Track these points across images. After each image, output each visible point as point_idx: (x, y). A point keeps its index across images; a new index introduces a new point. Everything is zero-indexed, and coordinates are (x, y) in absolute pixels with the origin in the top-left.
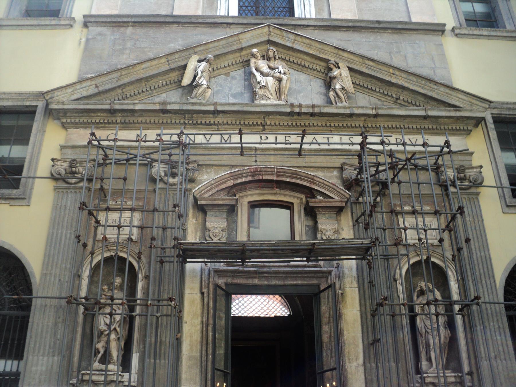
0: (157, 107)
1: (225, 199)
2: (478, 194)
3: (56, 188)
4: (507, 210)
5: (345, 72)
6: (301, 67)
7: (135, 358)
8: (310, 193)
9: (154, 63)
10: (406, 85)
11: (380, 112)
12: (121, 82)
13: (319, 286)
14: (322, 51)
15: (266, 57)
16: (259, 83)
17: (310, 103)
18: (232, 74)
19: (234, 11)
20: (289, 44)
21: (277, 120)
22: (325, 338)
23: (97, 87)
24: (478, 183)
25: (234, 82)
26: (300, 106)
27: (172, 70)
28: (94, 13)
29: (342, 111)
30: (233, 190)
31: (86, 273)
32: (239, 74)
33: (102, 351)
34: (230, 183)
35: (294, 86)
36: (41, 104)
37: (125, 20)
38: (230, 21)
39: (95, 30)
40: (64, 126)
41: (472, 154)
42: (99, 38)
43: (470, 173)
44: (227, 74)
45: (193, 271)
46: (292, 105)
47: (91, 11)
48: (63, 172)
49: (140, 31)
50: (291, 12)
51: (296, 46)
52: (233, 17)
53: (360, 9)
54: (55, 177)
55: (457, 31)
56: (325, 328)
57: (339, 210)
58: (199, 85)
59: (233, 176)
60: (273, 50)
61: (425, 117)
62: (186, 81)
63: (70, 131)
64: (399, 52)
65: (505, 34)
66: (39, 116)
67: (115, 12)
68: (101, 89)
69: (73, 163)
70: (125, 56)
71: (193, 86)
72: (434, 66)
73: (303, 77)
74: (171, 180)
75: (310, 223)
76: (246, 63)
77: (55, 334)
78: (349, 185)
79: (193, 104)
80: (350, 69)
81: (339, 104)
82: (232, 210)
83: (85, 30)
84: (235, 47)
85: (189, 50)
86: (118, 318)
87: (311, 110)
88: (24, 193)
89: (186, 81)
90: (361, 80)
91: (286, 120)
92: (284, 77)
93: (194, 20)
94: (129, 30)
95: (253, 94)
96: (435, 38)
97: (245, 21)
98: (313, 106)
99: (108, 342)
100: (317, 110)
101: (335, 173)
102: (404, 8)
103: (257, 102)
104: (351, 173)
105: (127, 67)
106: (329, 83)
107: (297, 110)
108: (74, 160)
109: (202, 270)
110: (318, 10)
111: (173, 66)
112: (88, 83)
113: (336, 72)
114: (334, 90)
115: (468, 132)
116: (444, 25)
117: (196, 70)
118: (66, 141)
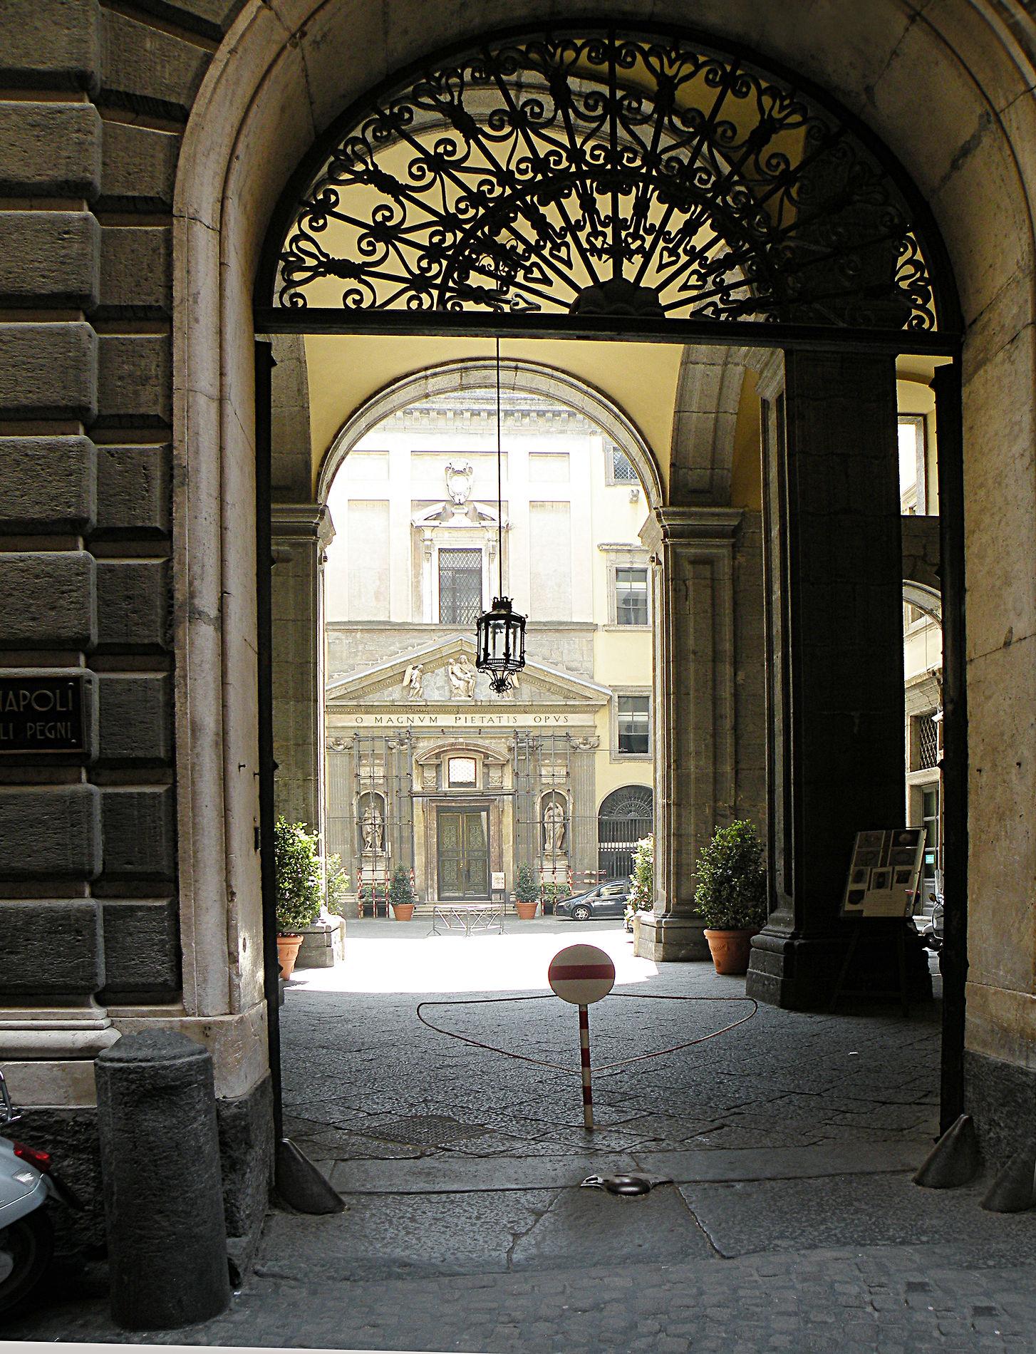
1: (435, 761)
8: (487, 756)
15: (458, 661)
30: (438, 756)
31: (354, 802)
44: (433, 672)
55: (607, 628)
94: (359, 635)
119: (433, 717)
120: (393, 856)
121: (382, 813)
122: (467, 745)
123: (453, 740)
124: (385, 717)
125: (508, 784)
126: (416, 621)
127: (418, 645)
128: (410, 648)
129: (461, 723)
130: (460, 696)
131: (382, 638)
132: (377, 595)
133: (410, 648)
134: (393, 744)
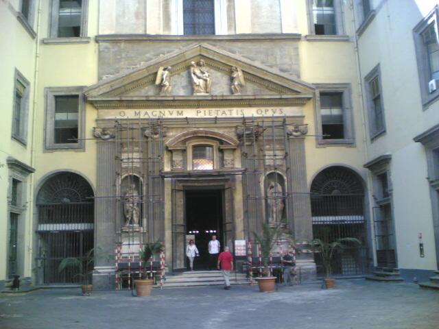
0: (144, 99)
1: (181, 147)
2: (304, 139)
3: (97, 143)
4: (319, 146)
5: (240, 74)
6: (218, 69)
7: (145, 221)
8: (221, 142)
9: (140, 71)
10: (272, 80)
11: (257, 97)
12: (124, 84)
13: (224, 186)
14: (230, 62)
15: (198, 64)
16: (195, 83)
17: (221, 94)
18: (182, 74)
19: (181, 32)
20: (211, 57)
21: (204, 103)
22: (227, 209)
23: (111, 87)
24: (304, 134)
25: (183, 79)
26: (216, 96)
27: (150, 75)
28: (101, 33)
29: (237, 98)
30: (184, 142)
32: (184, 74)
33: (130, 218)
34: (183, 138)
35: (214, 80)
36: (80, 93)
37: (120, 38)
38: (179, 38)
39: (103, 45)
40: (96, 108)
41: (303, 117)
42: (106, 50)
43: (301, 128)
44: (179, 74)
45: (168, 181)
46: (212, 96)
47: (98, 32)
48: (100, 134)
49: (129, 45)
50: (214, 33)
51: (215, 58)
52: (181, 36)
53: (253, 24)
54: (96, 137)
55: (308, 38)
56: (227, 204)
57: (234, 150)
58: (164, 86)
59: (184, 135)
60: (202, 61)
61: (281, 99)
62: (158, 82)
63: (100, 111)
64: (272, 55)
65: (338, 38)
66: (80, 101)
67: (113, 32)
68: (114, 88)
69: (104, 130)
70: (122, 63)
71: (161, 86)
72: (290, 63)
73: (219, 74)
74: (155, 136)
75: (221, 155)
76: (188, 67)
77: (108, 213)
78: (240, 137)
79: (162, 97)
80: (243, 71)
81: (236, 94)
82: (184, 151)
83: (97, 44)
84: (182, 60)
85: (158, 65)
86: (136, 204)
87: (221, 98)
88: (81, 145)
89: (158, 82)
90: (249, 77)
91: (209, 103)
92: (208, 79)
93: (159, 38)
94: (123, 45)
95: (193, 90)
96: (293, 44)
97: (187, 38)
98: (223, 96)
99: (132, 215)
100: (225, 98)
101: (234, 129)
102: (279, 22)
103: (195, 94)
104: (240, 130)
105: (126, 76)
106: (232, 79)
107: (214, 98)
108: (105, 128)
109: (172, 180)
110: (229, 27)
111: (150, 73)
112: (107, 85)
113: (235, 75)
114: (234, 85)
115: (303, 105)
116: (300, 35)
117: (162, 75)
118: (98, 115)
119: (180, 110)
120: (148, 231)
121: (140, 193)
122: (206, 132)
123: (195, 129)
124: (143, 111)
125: (238, 165)
126: (166, 33)
127: (168, 52)
128: (161, 55)
129: (201, 115)
130: (200, 92)
131: (140, 47)
132: (137, 15)
133: (161, 55)
134: (147, 132)
